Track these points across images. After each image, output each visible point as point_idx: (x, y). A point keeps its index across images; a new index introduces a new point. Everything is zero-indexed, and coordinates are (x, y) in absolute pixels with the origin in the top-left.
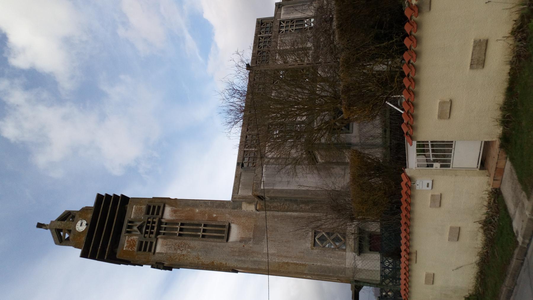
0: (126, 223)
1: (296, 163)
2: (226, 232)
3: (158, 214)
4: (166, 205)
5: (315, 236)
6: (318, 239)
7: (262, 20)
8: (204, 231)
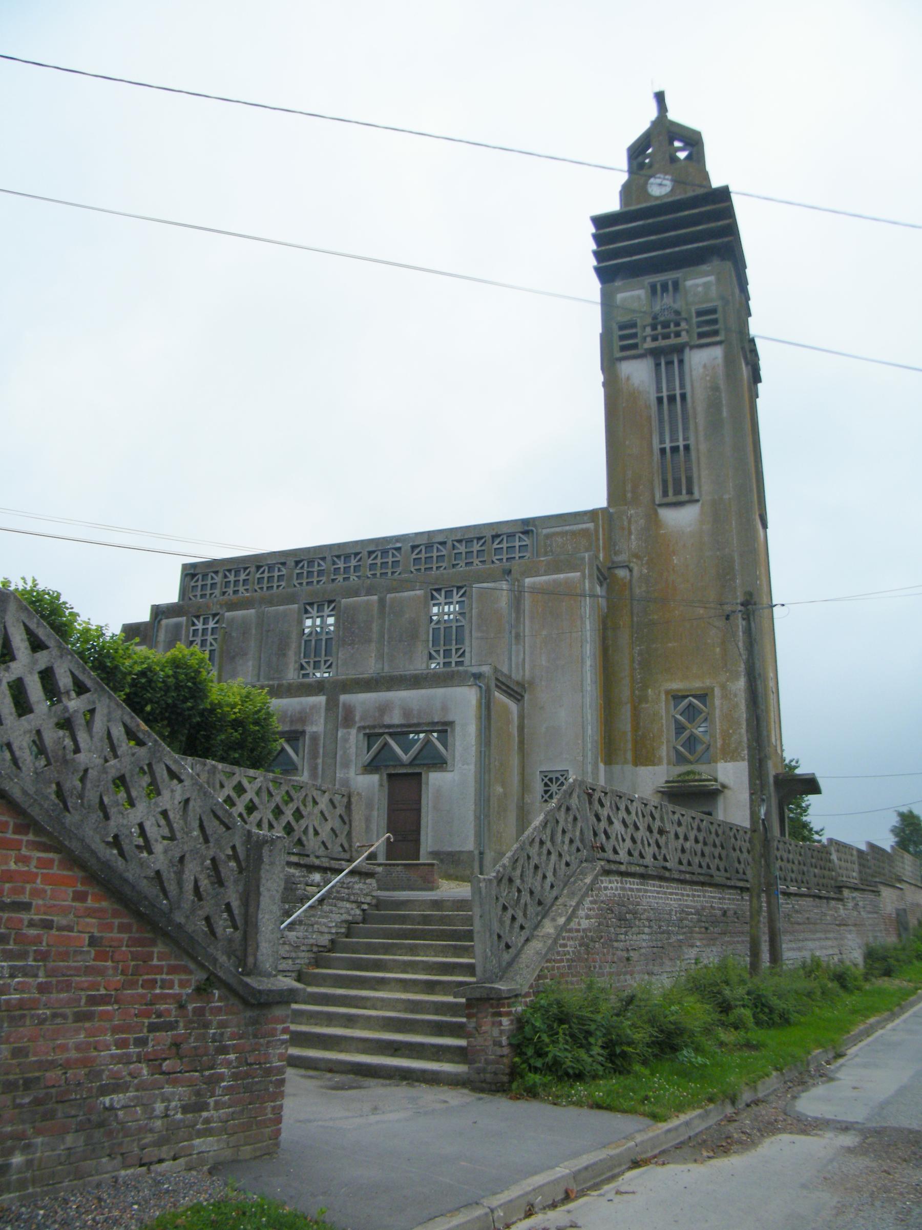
0: (668, 276)
1: (153, 783)
2: (666, 500)
3: (701, 335)
4: (723, 346)
5: (695, 696)
6: (690, 705)
7: (194, 566)
8: (675, 450)
